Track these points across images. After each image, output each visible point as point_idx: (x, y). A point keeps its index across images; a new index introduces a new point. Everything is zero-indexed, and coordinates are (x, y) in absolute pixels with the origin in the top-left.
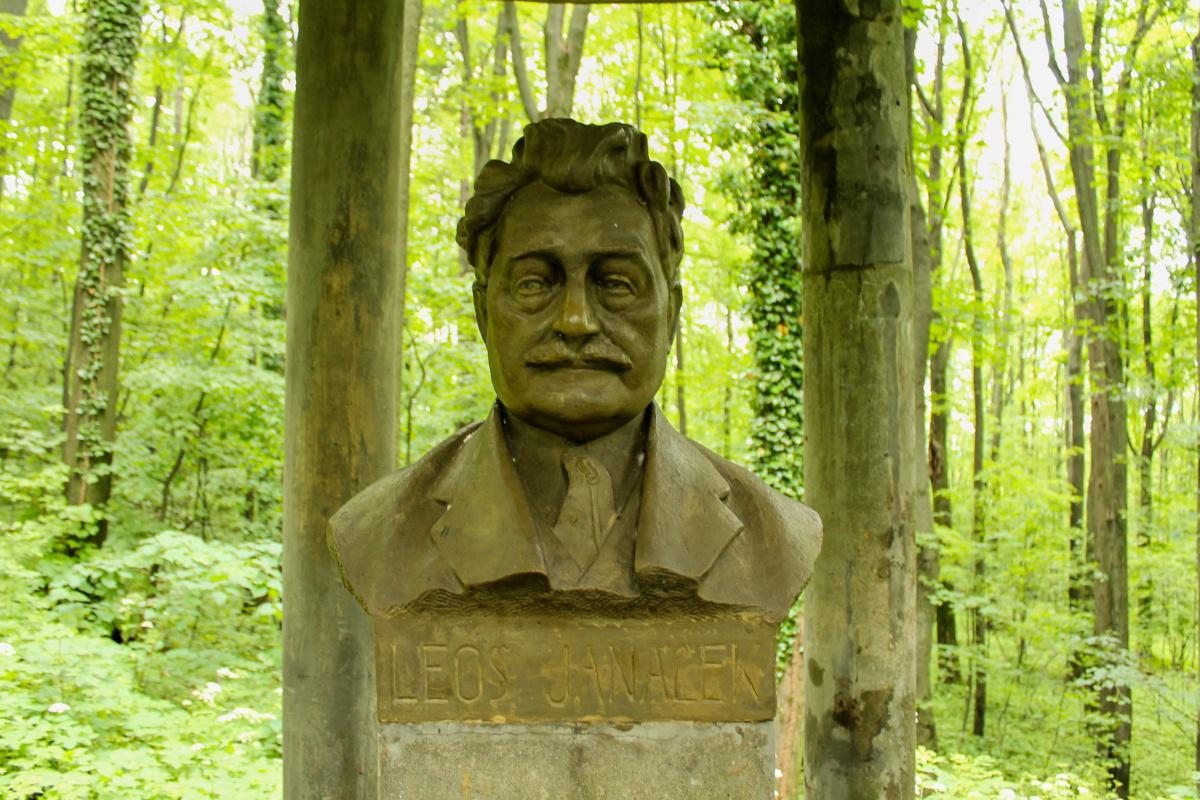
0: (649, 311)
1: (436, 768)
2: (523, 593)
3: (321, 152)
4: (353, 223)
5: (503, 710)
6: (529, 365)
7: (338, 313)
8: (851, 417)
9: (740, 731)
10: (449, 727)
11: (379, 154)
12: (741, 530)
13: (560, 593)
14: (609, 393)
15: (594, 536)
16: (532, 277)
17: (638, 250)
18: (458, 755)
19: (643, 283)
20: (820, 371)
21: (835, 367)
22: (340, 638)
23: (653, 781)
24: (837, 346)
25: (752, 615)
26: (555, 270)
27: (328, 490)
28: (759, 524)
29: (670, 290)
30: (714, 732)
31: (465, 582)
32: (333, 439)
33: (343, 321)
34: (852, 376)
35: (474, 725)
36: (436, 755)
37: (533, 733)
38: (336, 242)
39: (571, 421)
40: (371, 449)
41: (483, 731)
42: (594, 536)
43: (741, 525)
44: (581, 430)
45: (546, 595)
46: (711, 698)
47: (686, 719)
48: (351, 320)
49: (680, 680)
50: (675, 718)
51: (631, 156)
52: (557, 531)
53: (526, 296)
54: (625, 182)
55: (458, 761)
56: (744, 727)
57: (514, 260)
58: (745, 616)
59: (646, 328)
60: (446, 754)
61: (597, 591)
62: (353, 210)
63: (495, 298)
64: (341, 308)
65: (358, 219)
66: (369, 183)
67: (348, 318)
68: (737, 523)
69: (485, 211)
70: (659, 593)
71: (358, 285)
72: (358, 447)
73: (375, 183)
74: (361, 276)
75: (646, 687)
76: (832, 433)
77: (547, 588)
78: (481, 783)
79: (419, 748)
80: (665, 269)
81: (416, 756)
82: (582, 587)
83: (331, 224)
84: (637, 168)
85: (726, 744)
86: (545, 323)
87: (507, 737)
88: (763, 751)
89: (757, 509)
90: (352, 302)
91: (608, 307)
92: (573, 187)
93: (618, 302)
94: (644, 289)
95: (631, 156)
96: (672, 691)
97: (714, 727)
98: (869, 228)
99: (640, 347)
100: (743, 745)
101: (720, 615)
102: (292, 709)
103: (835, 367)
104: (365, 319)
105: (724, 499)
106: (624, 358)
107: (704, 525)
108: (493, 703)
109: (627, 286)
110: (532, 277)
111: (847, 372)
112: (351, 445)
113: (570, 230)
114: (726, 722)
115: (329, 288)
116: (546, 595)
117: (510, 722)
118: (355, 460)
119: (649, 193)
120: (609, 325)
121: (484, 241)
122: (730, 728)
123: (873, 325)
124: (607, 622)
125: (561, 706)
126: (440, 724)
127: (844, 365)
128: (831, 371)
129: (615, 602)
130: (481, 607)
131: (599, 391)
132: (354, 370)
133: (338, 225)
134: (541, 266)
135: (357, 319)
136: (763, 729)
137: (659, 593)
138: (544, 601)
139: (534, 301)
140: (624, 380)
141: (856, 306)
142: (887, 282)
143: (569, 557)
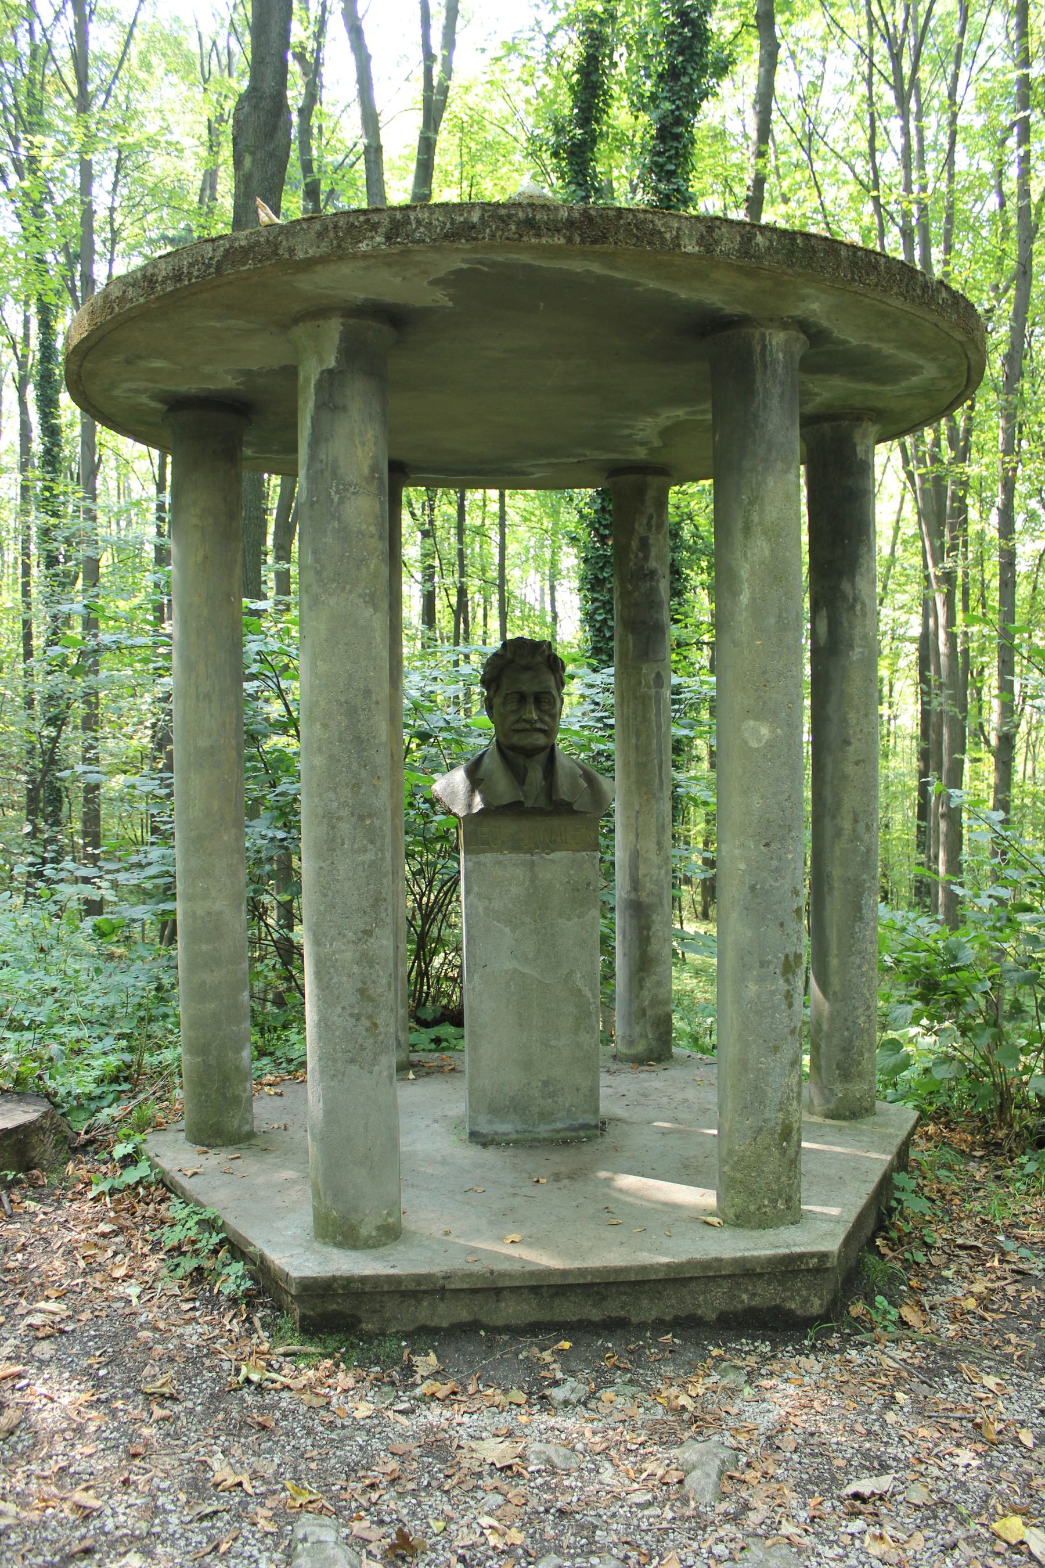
10: (489, 855)
14: (541, 740)
26: (522, 698)
30: (578, 855)
44: (529, 753)
79: (478, 863)
113: (527, 684)
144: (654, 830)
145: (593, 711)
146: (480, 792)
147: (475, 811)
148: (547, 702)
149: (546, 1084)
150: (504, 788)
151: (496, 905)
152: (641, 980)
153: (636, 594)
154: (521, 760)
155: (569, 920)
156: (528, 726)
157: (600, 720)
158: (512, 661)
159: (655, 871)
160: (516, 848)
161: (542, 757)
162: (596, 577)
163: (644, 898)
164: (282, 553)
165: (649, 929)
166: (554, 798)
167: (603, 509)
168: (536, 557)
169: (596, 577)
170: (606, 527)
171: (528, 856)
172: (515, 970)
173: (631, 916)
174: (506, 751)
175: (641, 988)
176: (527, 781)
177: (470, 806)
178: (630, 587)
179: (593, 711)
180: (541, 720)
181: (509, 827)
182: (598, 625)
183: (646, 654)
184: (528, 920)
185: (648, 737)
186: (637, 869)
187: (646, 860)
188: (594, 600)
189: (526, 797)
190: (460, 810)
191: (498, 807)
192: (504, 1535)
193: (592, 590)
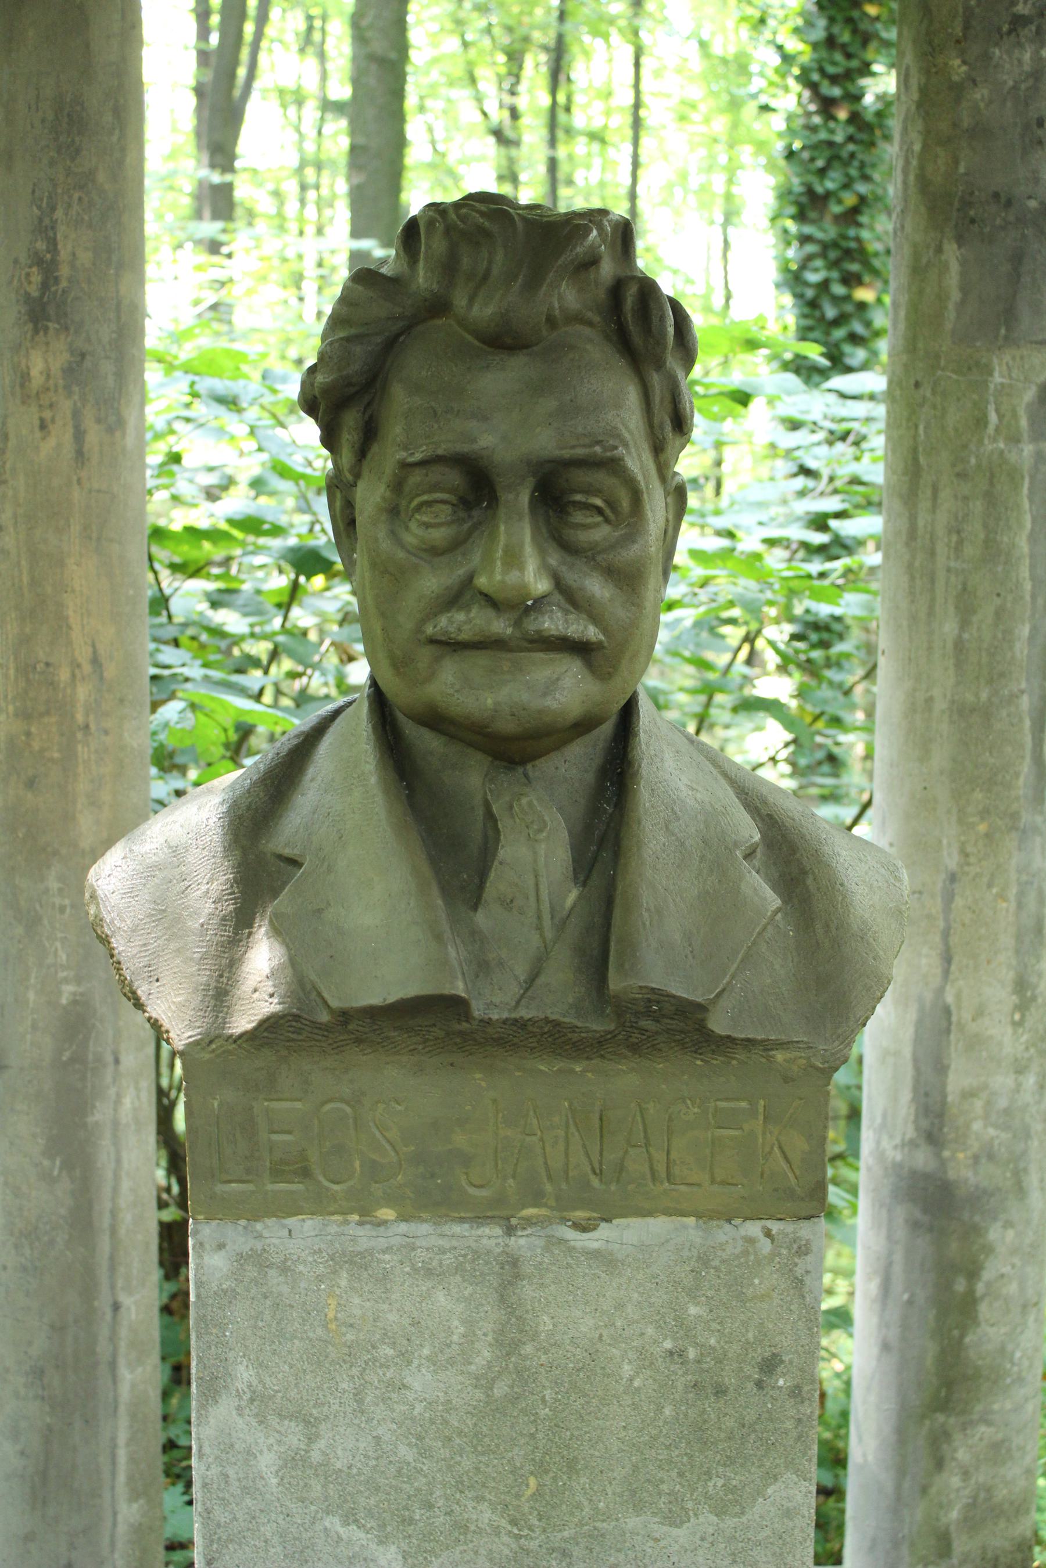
0: (632, 552)
1: (285, 1289)
4: (64, 254)
5: (389, 1201)
6: (432, 641)
7: (43, 426)
8: (964, 624)
9: (768, 1234)
10: (307, 1225)
11: (108, 118)
12: (779, 910)
14: (565, 689)
15: (539, 928)
16: (439, 496)
17: (621, 450)
18: (321, 1269)
19: (625, 504)
20: (912, 534)
21: (941, 532)
22: (64, 1001)
23: (629, 1309)
24: (945, 494)
25: (788, 1055)
26: (477, 487)
27: (36, 745)
29: (667, 494)
30: (728, 1236)
32: (41, 655)
33: (52, 442)
34: (970, 551)
35: (346, 1222)
36: (284, 1270)
37: (442, 1235)
38: (34, 291)
40: (110, 671)
41: (360, 1231)
42: (539, 928)
43: (778, 902)
44: (514, 749)
46: (724, 1183)
47: (684, 1214)
48: (68, 437)
49: (674, 1155)
50: (668, 1212)
51: (607, 269)
52: (481, 919)
53: (427, 526)
54: (597, 319)
55: (320, 1279)
56: (775, 1226)
58: (780, 1056)
60: (301, 1268)
61: (547, 1021)
62: (62, 229)
64: (47, 414)
65: (74, 247)
66: (91, 175)
67: (62, 435)
68: (772, 900)
69: (356, 367)
71: (77, 370)
72: (87, 668)
73: (101, 177)
74: (83, 355)
75: (621, 1168)
76: (930, 648)
77: (467, 1016)
78: (358, 1312)
79: (258, 1259)
81: (251, 1272)
82: (524, 1013)
83: (23, 259)
84: (617, 289)
85: (746, 1253)
87: (396, 1241)
88: (803, 1264)
89: (804, 872)
90: (66, 406)
91: (567, 547)
92: (509, 341)
93: (584, 537)
94: (628, 513)
95: (607, 269)
96: (661, 1169)
97: (727, 1226)
98: (1015, 276)
99: (619, 612)
100: (773, 1255)
101: (741, 1055)
103: (941, 532)
104: (93, 436)
105: (748, 856)
108: (378, 1190)
109: (600, 511)
110: (439, 496)
111: (960, 542)
112: (76, 665)
113: (506, 420)
114: (746, 1219)
117: (403, 1218)
118: (82, 692)
119: (637, 339)
120: (571, 578)
121: (351, 420)
122: (753, 1229)
123: (1013, 457)
124: (559, 1065)
126: (291, 1221)
127: (956, 529)
128: (932, 541)
129: (575, 1037)
130: (359, 1041)
131: (550, 688)
132: (75, 528)
133: (38, 260)
134: (454, 478)
135: (79, 435)
136: (805, 1230)
137: (646, 1023)
138: (461, 1033)
140: (589, 665)
141: (981, 422)
143: (501, 964)
144: (1007, 940)
145: (802, 493)
146: (277, 931)
147: (242, 1023)
148: (595, 504)
150: (384, 928)
151: (342, 1446)
152: (939, 1440)
153: (980, 94)
154: (472, 778)
155: (674, 1519)
156: (500, 626)
157: (820, 522)
158: (437, 307)
159: (1002, 1081)
160: (435, 1195)
161: (575, 765)
162: (810, 192)
163: (962, 1169)
164: (219, 159)
165: (973, 1274)
166: (615, 983)
167: (830, 42)
168: (703, 189)
169: (810, 192)
170: (834, 79)
171: (489, 1236)
173: (915, 1225)
174: (411, 730)
175: (939, 1464)
176: (496, 884)
177: (220, 994)
178: (958, 69)
179: (802, 493)
180: (569, 596)
181: (399, 1096)
182: (810, 293)
183: (1009, 315)
184: (486, 1515)
185: (999, 614)
186: (941, 1069)
187: (975, 1043)
188: (805, 239)
189: (482, 967)
190: (174, 1008)
191: (345, 1016)
192: (771, 402)
193: (801, 217)
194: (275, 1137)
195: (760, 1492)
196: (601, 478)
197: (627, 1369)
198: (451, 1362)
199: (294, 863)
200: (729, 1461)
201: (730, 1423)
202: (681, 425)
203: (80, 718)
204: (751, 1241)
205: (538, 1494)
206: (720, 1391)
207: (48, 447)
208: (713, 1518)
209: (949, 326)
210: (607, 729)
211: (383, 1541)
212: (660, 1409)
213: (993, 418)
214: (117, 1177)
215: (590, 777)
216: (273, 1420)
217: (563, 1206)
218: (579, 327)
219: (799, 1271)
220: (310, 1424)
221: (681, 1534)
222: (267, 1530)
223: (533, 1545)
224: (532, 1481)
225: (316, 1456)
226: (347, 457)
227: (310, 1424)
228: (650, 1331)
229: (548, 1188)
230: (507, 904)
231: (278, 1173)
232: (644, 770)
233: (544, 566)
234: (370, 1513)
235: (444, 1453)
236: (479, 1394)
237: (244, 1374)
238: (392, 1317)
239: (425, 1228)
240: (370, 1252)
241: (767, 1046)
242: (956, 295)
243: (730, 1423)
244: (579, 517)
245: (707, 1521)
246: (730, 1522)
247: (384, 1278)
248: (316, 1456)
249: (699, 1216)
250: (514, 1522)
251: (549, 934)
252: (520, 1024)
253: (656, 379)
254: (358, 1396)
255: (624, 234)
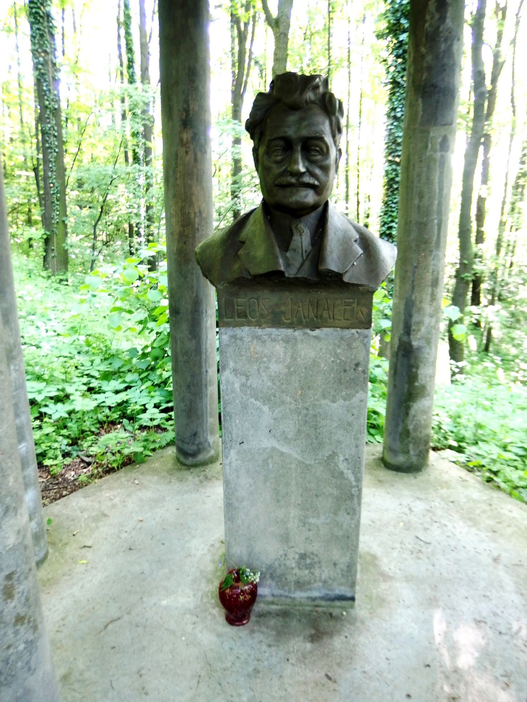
2: (274, 279)
3: (174, 72)
4: (191, 108)
5: (266, 322)
6: (277, 185)
8: (420, 201)
9: (357, 332)
10: (246, 329)
13: (289, 278)
14: (310, 197)
26: (288, 145)
27: (186, 234)
28: (369, 251)
29: (337, 150)
31: (252, 274)
38: (184, 118)
39: (292, 202)
42: (302, 256)
45: (283, 279)
46: (347, 320)
48: (193, 156)
50: (333, 327)
51: (321, 90)
52: (288, 254)
56: (359, 331)
57: (270, 141)
58: (361, 288)
59: (325, 169)
63: (263, 156)
64: (187, 149)
68: (360, 251)
69: (257, 117)
70: (328, 279)
75: (321, 316)
79: (234, 337)
80: (335, 142)
81: (233, 340)
83: (181, 109)
85: (351, 337)
86: (284, 168)
94: (326, 153)
100: (359, 337)
102: (174, 326)
105: (356, 241)
106: (316, 183)
107: (346, 252)
109: (318, 151)
112: (195, 213)
115: (182, 140)
116: (283, 279)
119: (329, 108)
120: (311, 169)
121: (257, 131)
122: (354, 331)
125: (288, 321)
126: (242, 328)
131: (306, 196)
134: (282, 143)
137: (328, 279)
139: (279, 158)
142: (443, 134)
149: (303, 556)
161: (312, 218)
172: (274, 449)
176: (293, 245)
184: (288, 399)
194: (239, 308)
195: (354, 395)
196: (318, 142)
197: (322, 365)
198: (280, 362)
199: (243, 243)
200: (347, 388)
201: (347, 378)
202: (340, 131)
203: (196, 226)
204: (353, 334)
205: (301, 395)
206: (345, 371)
207: (188, 157)
208: (343, 401)
209: (419, 121)
210: (320, 209)
211: (264, 404)
212: (330, 375)
213: (430, 145)
214: (206, 341)
215: (316, 222)
216: (238, 375)
217: (306, 326)
218: (313, 105)
219: (365, 342)
220: (247, 377)
221: (335, 405)
222: (237, 401)
223: (300, 407)
224: (300, 392)
225: (248, 384)
226: (256, 140)
227: (247, 377)
228: (328, 356)
229: (304, 320)
230: (295, 250)
231: (239, 316)
232: (329, 219)
233: (304, 165)
234: (261, 398)
235: (279, 384)
236: (287, 370)
237: (232, 364)
238: (266, 351)
239: (274, 330)
240: (261, 335)
241: (358, 285)
242: (421, 113)
243: (347, 378)
244: (313, 153)
245: (341, 402)
246: (347, 403)
247: (264, 342)
248: (248, 384)
249: (341, 328)
250: (295, 401)
251: (305, 257)
252: (297, 279)
253: (334, 119)
254: (258, 370)
255: (326, 82)
